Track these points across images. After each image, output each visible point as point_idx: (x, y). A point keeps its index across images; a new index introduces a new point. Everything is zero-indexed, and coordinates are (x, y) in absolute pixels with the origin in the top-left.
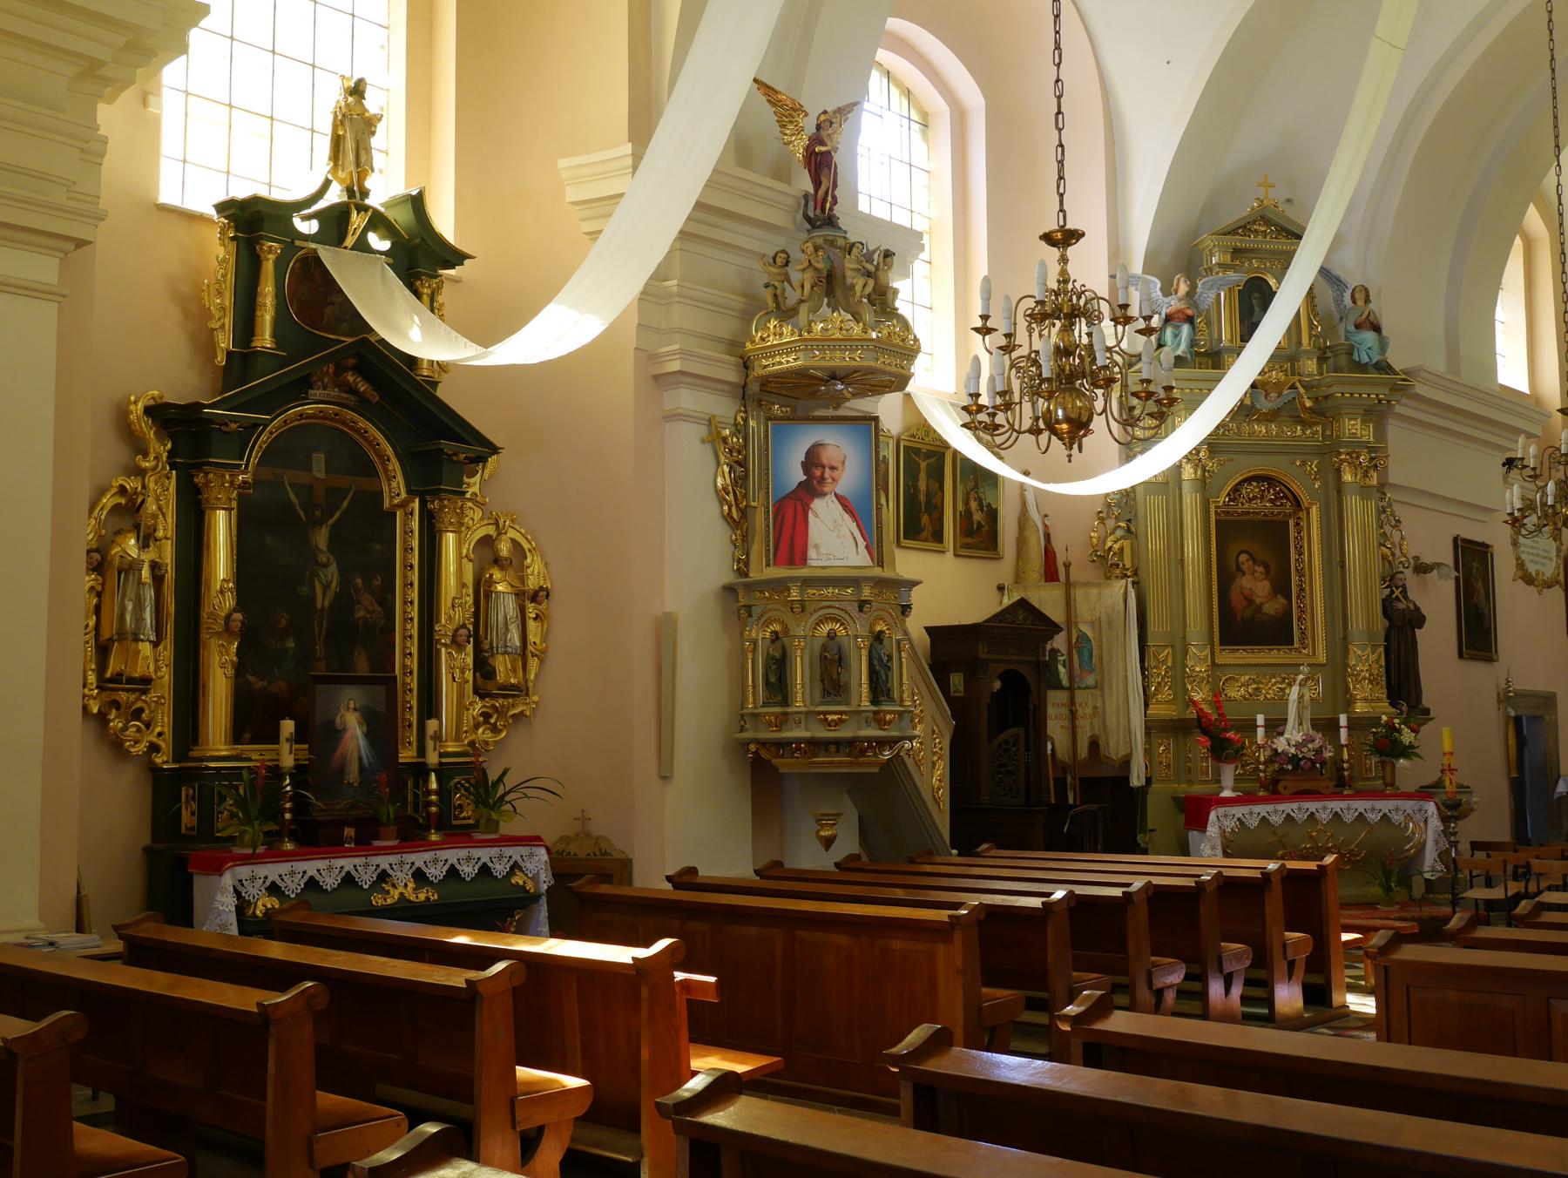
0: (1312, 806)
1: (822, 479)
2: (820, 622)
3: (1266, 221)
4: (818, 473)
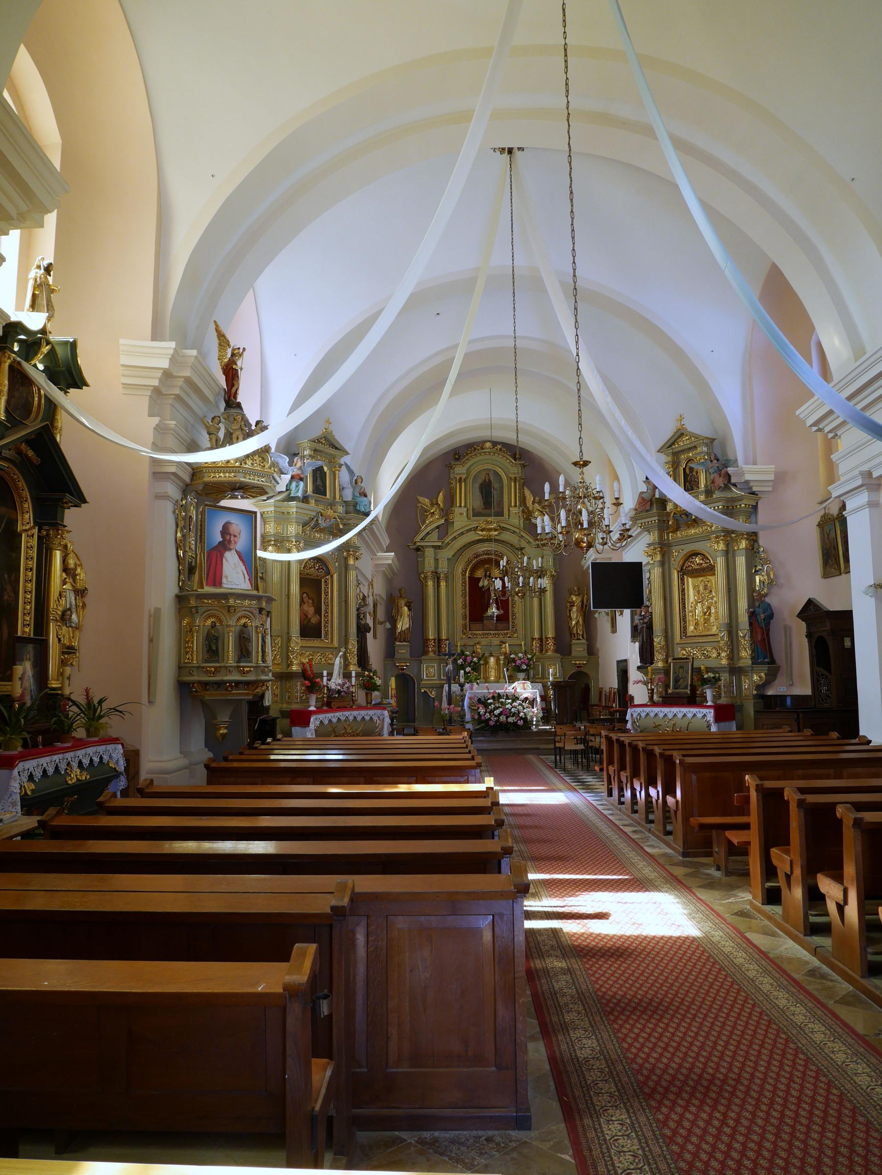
0: (347, 713)
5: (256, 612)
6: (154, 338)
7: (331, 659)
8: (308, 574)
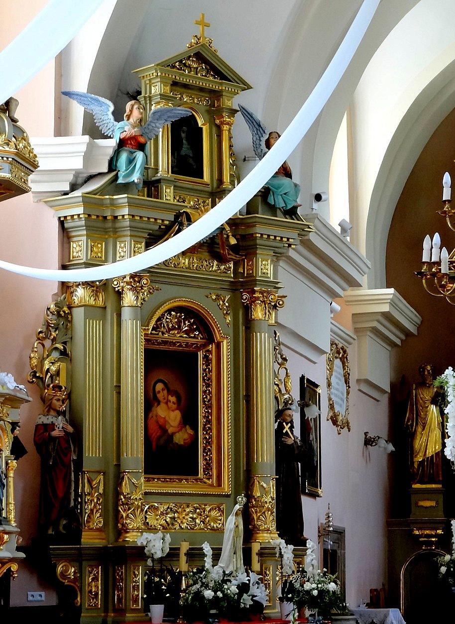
3: (199, 57)
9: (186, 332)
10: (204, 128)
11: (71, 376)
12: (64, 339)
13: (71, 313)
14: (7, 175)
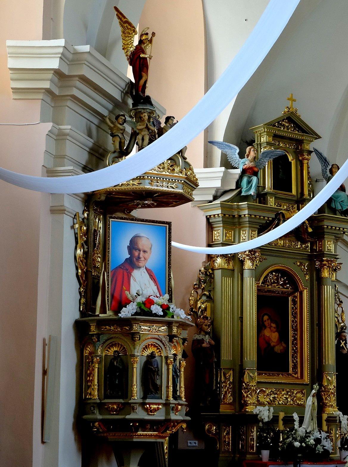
1: (139, 258)
2: (146, 347)
4: (136, 254)
5: (166, 340)
6: (46, 37)
7: (300, 399)
8: (269, 291)
9: (282, 285)
10: (293, 162)
11: (213, 312)
12: (209, 288)
13: (213, 273)
14: (181, 191)
